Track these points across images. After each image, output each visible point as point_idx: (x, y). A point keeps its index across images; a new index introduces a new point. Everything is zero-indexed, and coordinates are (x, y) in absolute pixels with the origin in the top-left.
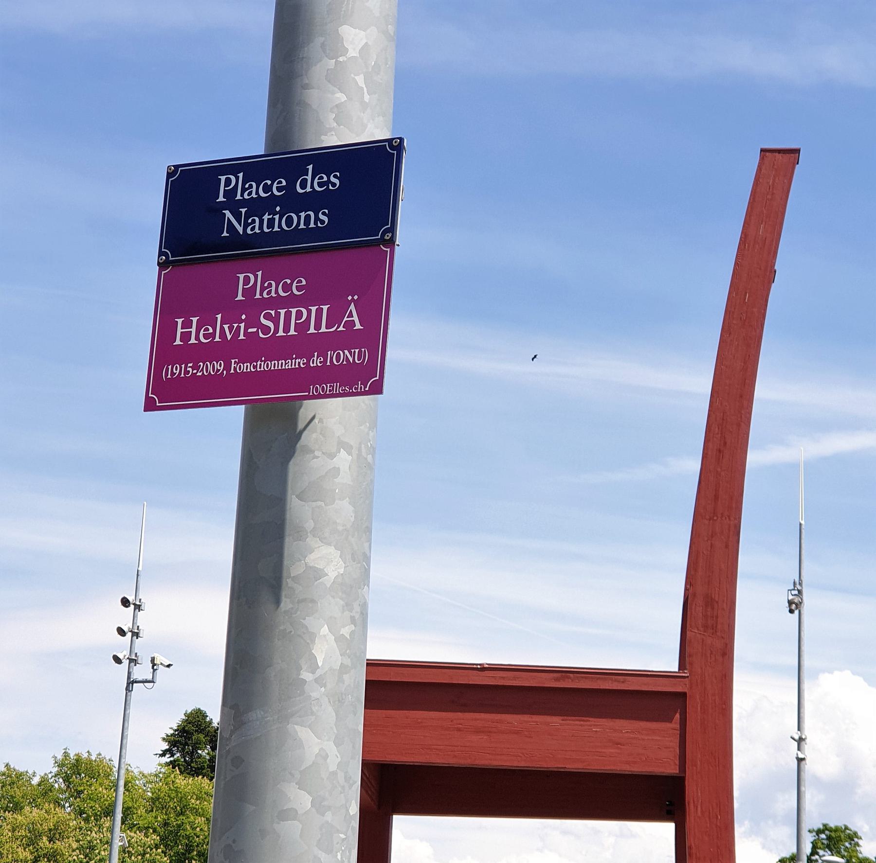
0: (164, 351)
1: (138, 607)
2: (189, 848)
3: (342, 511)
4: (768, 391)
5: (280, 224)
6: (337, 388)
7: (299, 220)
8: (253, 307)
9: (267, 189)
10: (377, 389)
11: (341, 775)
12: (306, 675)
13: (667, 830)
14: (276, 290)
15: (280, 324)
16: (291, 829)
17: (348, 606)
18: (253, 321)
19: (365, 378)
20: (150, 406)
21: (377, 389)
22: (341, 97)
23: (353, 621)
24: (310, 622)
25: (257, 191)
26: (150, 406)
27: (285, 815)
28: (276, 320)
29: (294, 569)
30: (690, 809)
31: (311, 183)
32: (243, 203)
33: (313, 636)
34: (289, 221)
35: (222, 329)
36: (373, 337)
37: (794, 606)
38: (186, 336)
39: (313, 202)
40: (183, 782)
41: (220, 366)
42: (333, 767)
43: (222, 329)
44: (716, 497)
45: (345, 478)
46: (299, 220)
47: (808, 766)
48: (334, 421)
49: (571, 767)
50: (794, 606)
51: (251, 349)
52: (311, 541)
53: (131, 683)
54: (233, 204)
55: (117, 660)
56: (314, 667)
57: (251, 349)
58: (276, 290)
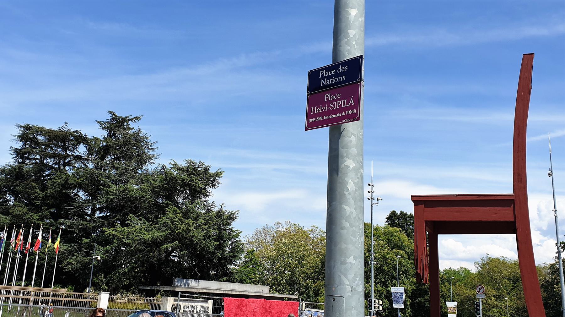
0: (309, 116)
1: (373, 186)
2: (394, 245)
3: (354, 151)
4: (532, 118)
5: (334, 81)
6: (349, 120)
7: (338, 79)
8: (329, 102)
9: (331, 73)
10: (358, 119)
11: (357, 218)
12: (345, 193)
13: (515, 235)
14: (334, 97)
15: (335, 106)
16: (344, 232)
17: (356, 174)
18: (329, 106)
19: (355, 117)
20: (306, 129)
21: (358, 119)
22: (349, 48)
23: (358, 178)
24: (346, 179)
25: (328, 74)
26: (306, 129)
27: (343, 228)
28: (334, 105)
29: (342, 166)
30: (518, 230)
31: (341, 70)
32: (326, 77)
33: (347, 182)
34: (336, 80)
35: (322, 109)
36: (357, 106)
37: (550, 175)
38: (314, 112)
39: (341, 74)
40: (392, 229)
41: (322, 118)
42: (354, 216)
43: (322, 109)
44: (519, 147)
45: (354, 142)
46: (338, 79)
47: (558, 218)
48: (351, 129)
49: (489, 220)
50: (550, 175)
51: (329, 113)
52: (345, 159)
53: (372, 204)
54: (323, 78)
55: (369, 199)
56: (348, 190)
57: (329, 113)
58: (334, 97)
